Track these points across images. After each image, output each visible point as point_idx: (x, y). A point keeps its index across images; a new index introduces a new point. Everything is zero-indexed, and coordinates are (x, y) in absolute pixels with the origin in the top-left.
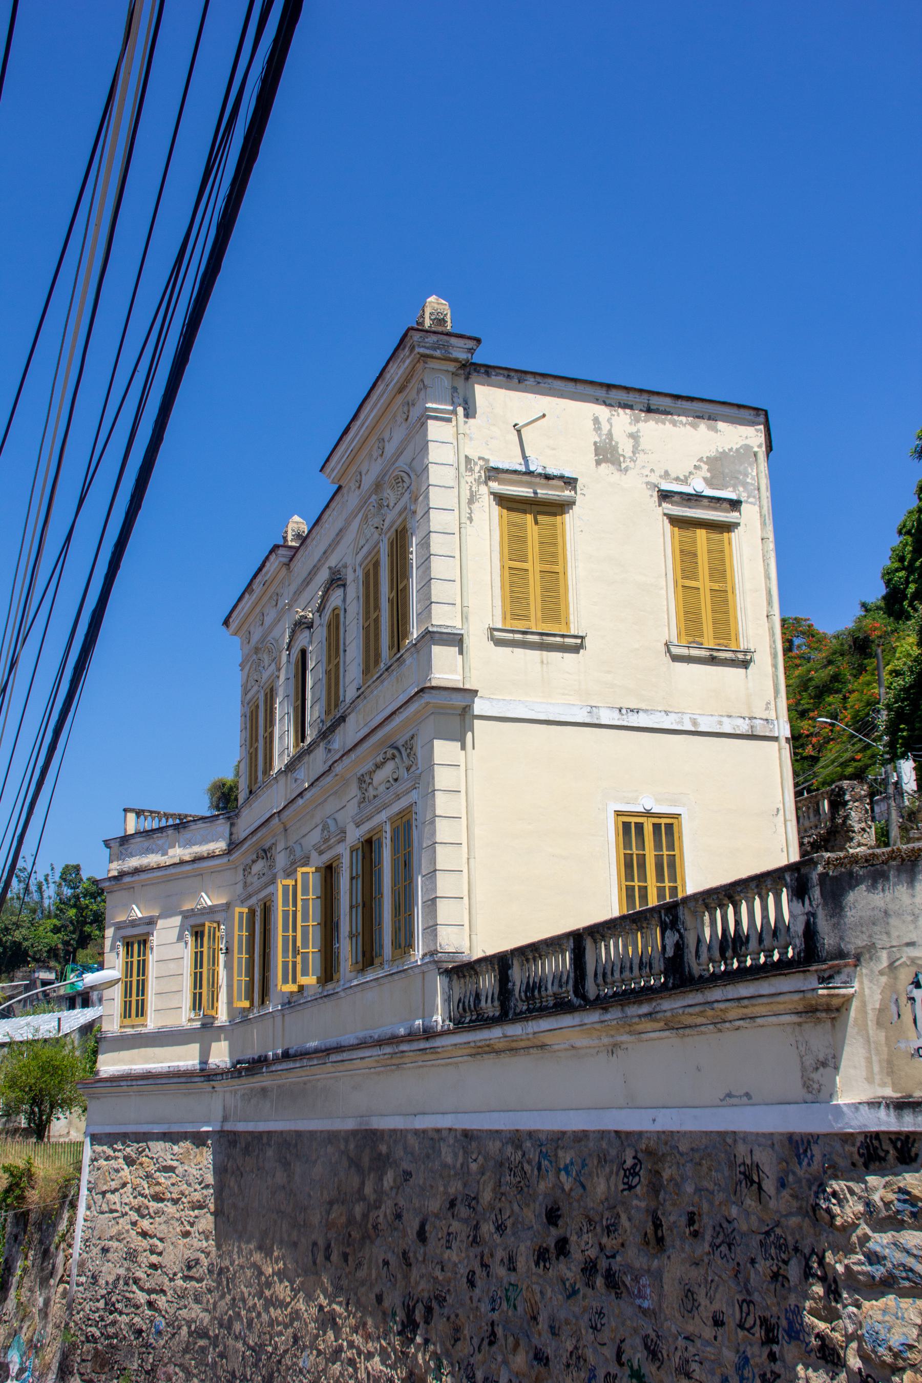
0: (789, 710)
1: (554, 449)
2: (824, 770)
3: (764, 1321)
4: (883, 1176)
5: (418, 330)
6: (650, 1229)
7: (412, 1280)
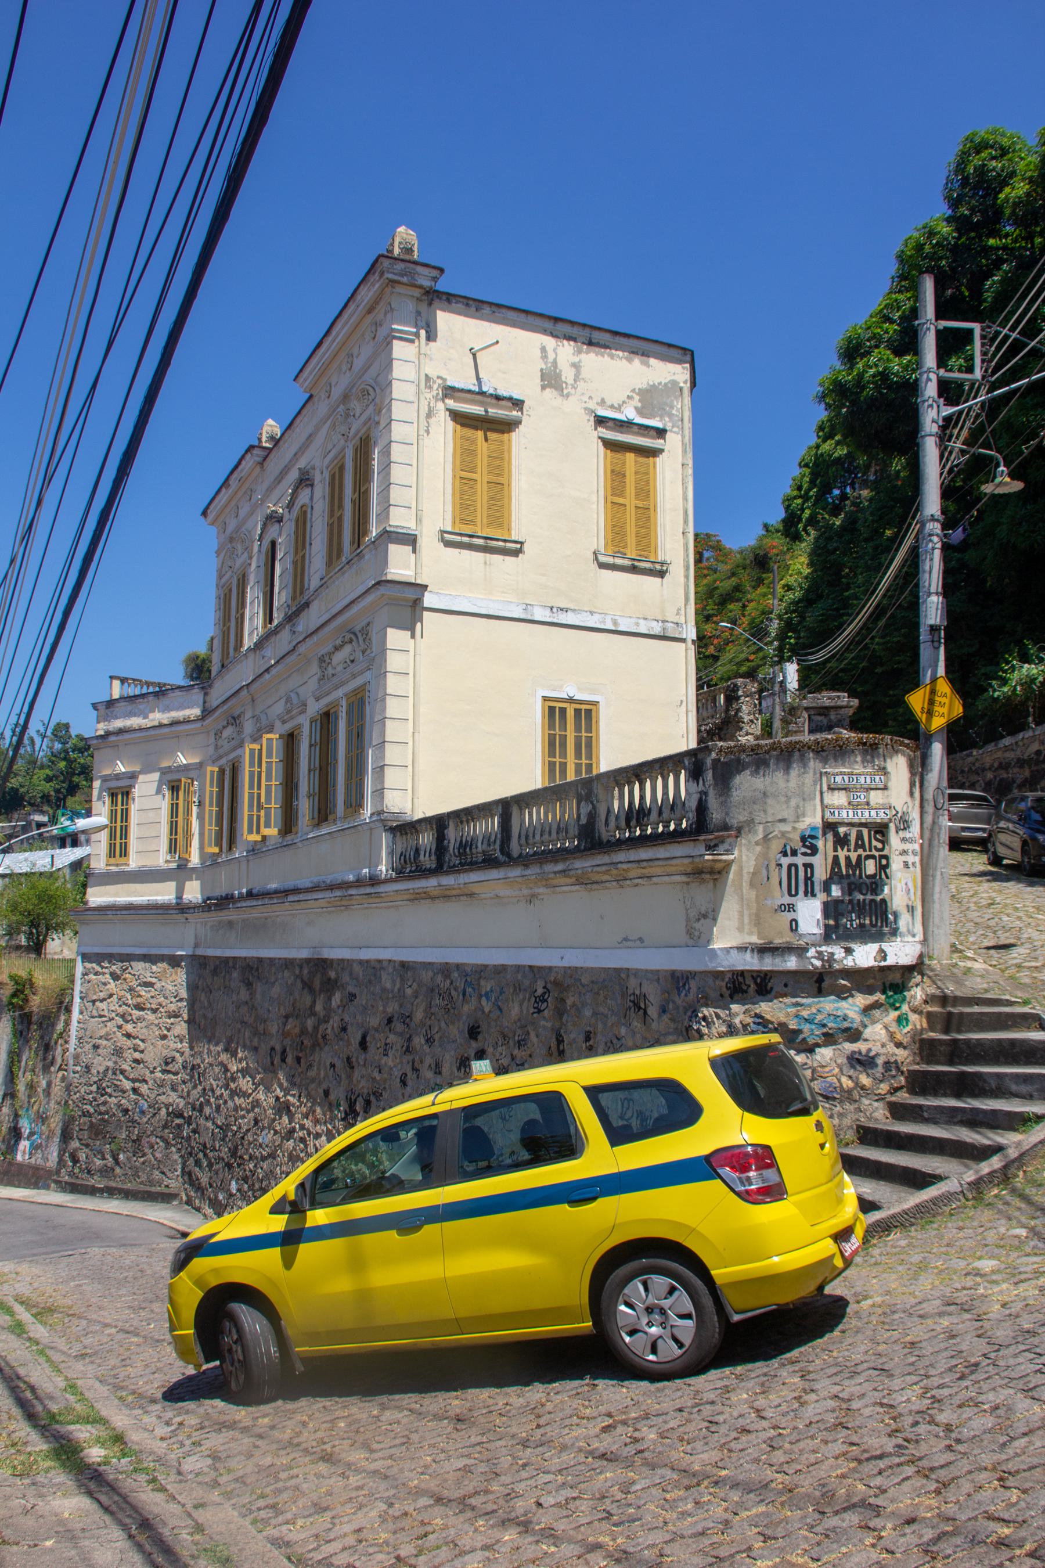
0: (696, 614)
1: (504, 373)
2: (722, 668)
6: (554, 1044)
7: (354, 1079)
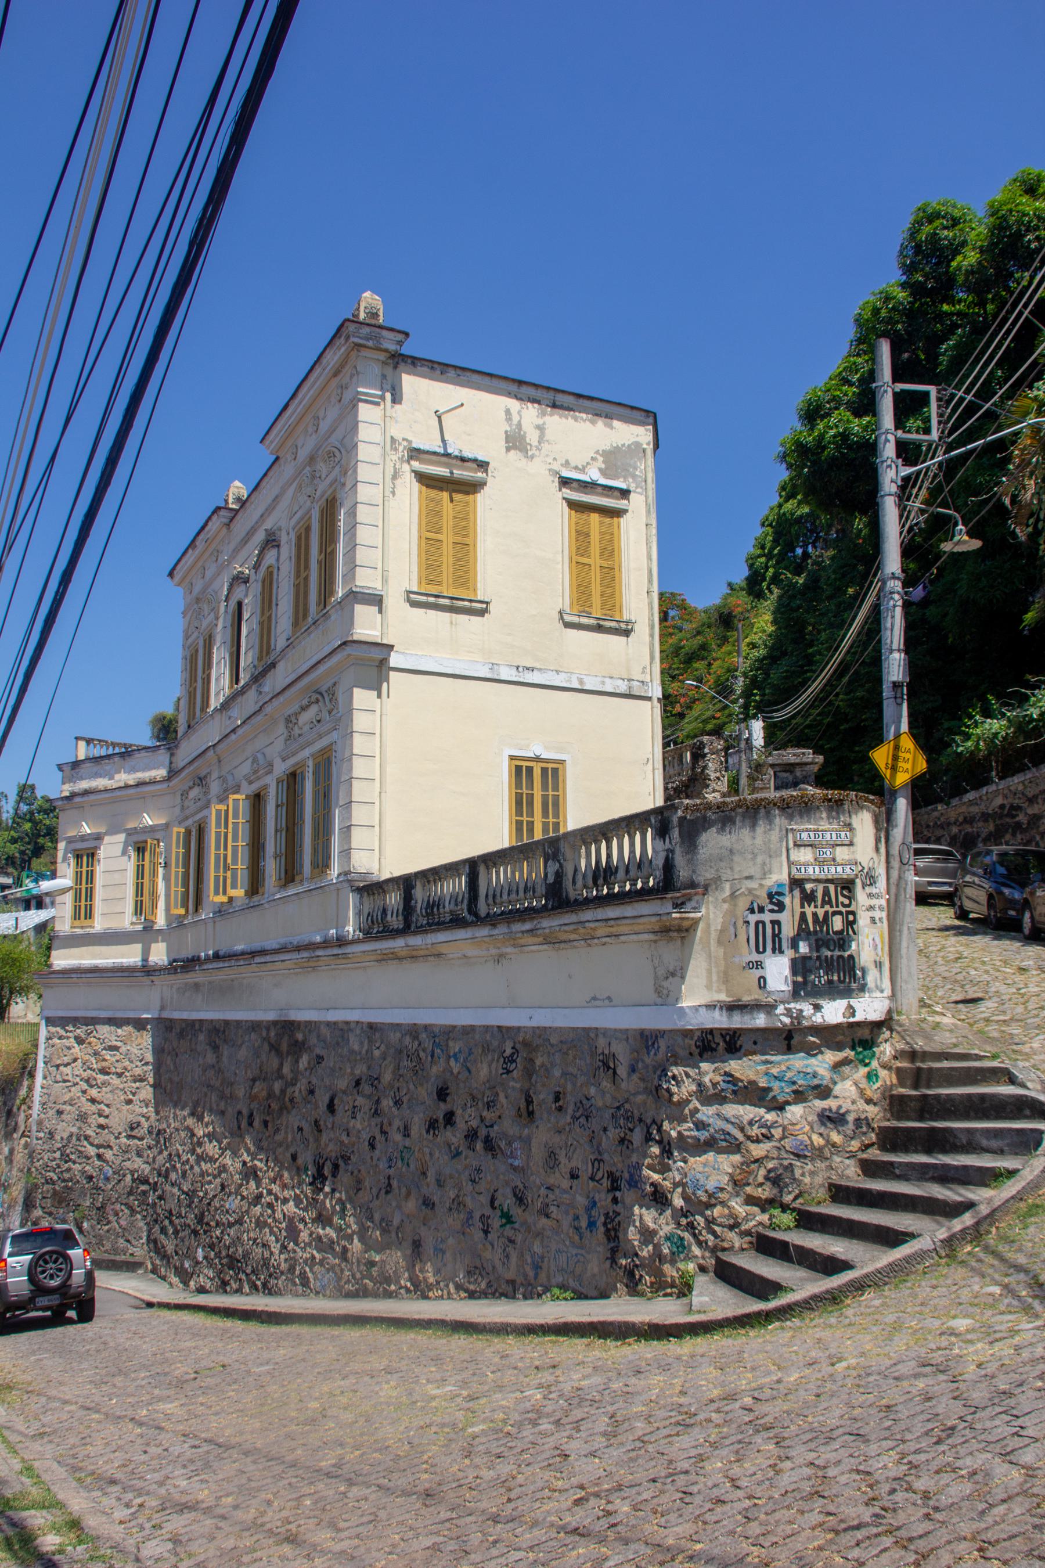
0: (662, 672)
2: (688, 726)
3: (610, 1175)
4: (713, 1063)
5: (353, 321)
6: (523, 1105)
